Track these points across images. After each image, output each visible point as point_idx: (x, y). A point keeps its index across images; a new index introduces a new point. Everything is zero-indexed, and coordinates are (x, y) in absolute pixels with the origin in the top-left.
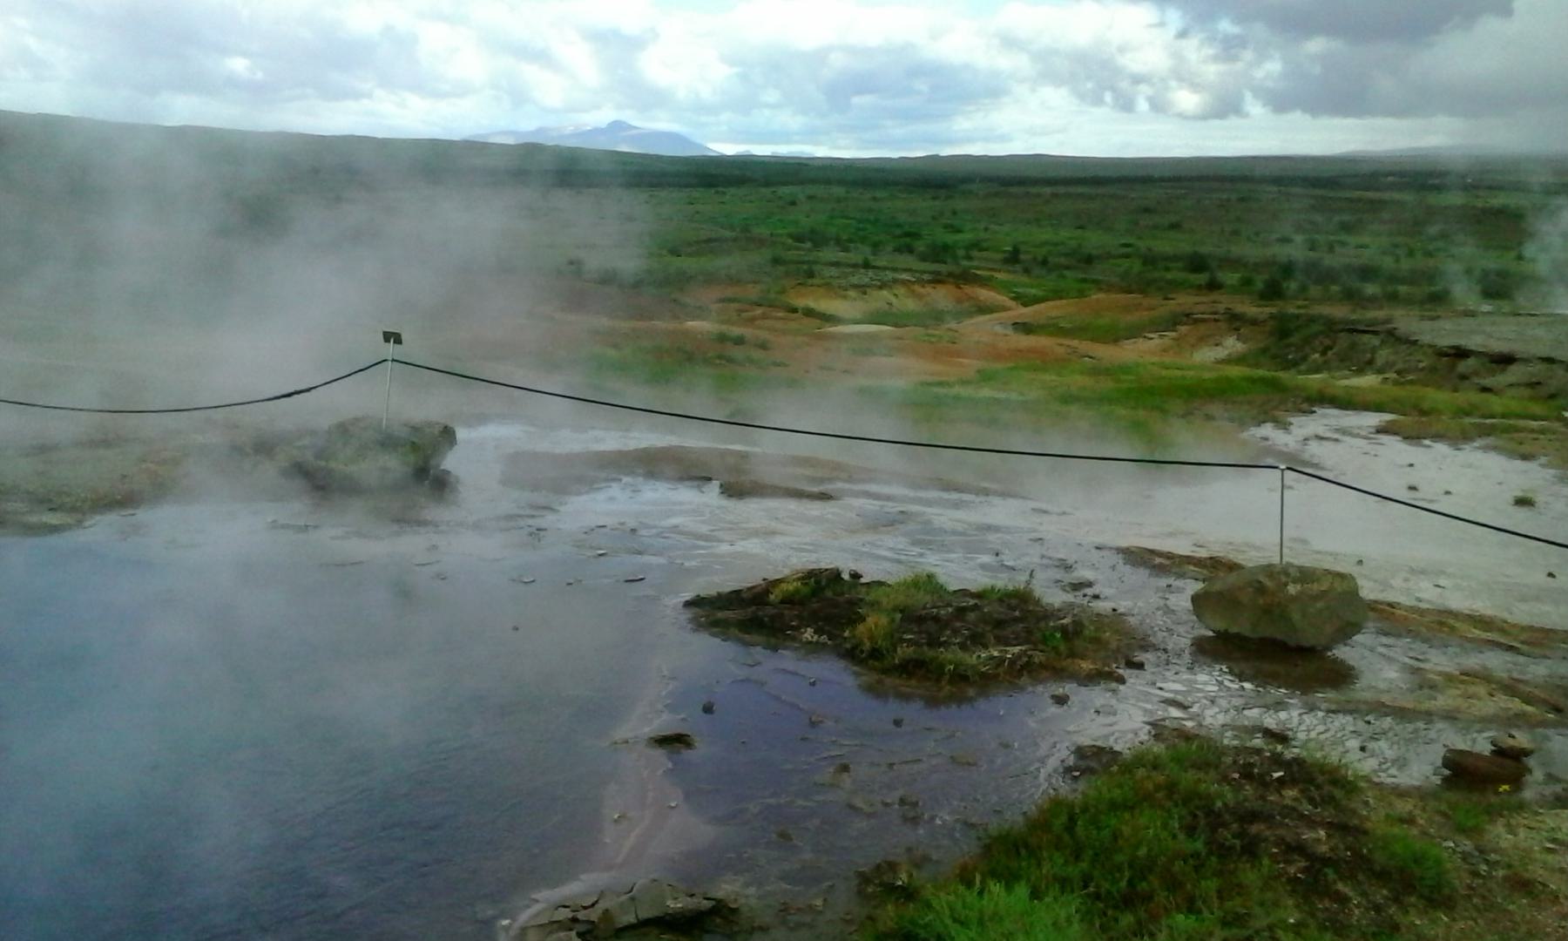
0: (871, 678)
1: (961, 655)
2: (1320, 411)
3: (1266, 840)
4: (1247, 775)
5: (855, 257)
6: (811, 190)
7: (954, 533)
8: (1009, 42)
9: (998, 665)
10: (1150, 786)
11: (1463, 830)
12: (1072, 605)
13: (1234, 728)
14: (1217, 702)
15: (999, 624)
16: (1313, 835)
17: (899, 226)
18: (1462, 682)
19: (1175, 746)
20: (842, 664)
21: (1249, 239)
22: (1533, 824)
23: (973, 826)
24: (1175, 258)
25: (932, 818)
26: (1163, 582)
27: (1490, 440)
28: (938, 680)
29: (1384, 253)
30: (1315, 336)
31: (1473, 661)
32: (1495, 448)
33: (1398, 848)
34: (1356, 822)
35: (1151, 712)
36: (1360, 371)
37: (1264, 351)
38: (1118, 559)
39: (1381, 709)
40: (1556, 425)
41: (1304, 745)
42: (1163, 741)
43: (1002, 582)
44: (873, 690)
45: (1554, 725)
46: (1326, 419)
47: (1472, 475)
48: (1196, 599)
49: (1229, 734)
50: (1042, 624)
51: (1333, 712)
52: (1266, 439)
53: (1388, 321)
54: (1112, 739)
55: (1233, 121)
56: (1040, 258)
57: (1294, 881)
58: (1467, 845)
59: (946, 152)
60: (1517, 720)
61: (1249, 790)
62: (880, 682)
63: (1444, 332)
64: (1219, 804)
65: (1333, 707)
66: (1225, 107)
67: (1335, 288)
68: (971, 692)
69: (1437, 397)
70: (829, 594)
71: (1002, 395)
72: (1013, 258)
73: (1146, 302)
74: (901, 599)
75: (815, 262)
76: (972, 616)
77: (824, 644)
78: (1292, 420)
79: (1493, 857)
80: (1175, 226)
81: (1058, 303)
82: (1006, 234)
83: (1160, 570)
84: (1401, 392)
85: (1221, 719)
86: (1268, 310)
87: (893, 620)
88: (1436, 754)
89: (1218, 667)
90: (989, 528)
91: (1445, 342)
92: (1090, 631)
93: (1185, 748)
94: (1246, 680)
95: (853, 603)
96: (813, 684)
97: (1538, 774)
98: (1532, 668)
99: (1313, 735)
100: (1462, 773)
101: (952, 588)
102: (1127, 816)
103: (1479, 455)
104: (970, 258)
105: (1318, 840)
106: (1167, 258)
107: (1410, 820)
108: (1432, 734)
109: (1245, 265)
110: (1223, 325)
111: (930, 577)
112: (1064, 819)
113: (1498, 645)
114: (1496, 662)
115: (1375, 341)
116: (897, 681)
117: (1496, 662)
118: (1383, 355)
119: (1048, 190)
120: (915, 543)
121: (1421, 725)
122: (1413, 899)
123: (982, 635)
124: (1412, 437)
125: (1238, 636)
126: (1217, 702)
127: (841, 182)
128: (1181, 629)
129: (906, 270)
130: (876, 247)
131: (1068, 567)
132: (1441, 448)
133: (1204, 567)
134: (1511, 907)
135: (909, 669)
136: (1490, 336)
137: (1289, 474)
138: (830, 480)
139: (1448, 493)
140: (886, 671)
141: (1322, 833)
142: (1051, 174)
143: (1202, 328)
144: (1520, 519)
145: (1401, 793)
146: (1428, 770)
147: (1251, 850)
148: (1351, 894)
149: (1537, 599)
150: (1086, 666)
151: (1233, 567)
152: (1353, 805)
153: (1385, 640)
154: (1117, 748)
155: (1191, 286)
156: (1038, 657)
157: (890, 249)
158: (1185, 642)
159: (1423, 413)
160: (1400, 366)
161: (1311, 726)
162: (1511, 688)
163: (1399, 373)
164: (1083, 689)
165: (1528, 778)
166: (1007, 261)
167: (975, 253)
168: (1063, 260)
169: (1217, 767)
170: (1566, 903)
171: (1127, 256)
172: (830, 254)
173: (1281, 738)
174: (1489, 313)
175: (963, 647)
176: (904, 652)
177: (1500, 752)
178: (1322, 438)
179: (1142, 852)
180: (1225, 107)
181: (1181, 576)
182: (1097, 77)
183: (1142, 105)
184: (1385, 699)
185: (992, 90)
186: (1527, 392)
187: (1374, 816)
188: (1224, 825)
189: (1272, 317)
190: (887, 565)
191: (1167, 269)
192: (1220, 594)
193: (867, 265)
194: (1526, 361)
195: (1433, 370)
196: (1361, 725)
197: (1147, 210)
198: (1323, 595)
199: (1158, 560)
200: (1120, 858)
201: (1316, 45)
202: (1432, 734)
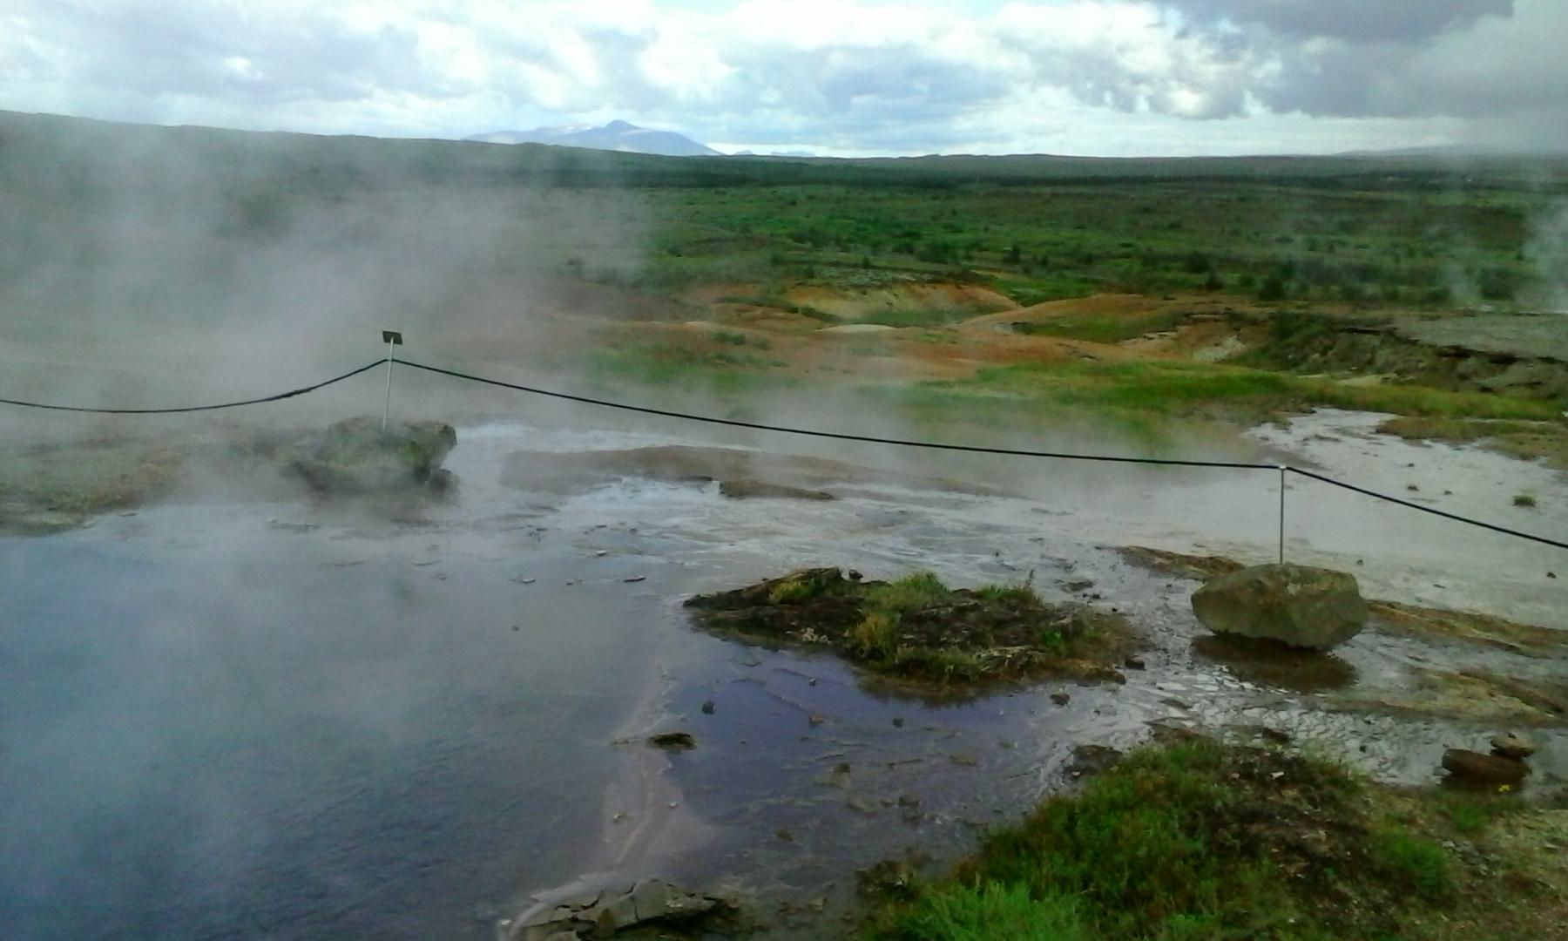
0: (871, 678)
1: (961, 655)
2: (1320, 411)
3: (1266, 840)
4: (1247, 775)
5: (855, 257)
6: (811, 190)
7: (954, 533)
8: (1009, 42)
9: (998, 665)
10: (1150, 786)
11: (1463, 830)
12: (1072, 605)
13: (1234, 728)
14: (1217, 702)
15: (999, 624)
16: (1313, 835)
17: (899, 226)
18: (1462, 682)
19: (1175, 746)
20: (842, 664)
21: (1249, 239)
22: (1533, 824)
23: (973, 826)
24: (1175, 258)
25: (932, 818)
26: (1163, 582)
27: (1490, 440)
28: (938, 680)
29: (1384, 253)
31: (1473, 661)
32: (1495, 448)
33: (1398, 848)
34: (1356, 822)
35: (1151, 712)
36: (1360, 371)
37: (1264, 351)
38: (1118, 559)
39: (1381, 709)
40: (1556, 425)
41: (1304, 745)
42: (1163, 741)
43: (1002, 582)
44: (873, 690)
45: (1554, 725)
46: (1326, 419)
47: (1472, 475)
48: (1196, 599)
49: (1229, 734)
50: (1042, 624)
51: (1333, 712)
52: (1266, 439)
53: (1388, 321)
54: (1112, 739)
55: (1233, 121)
56: (1040, 258)
57: (1294, 881)
58: (1467, 845)
59: (946, 152)
60: (1517, 720)
61: (1249, 790)
62: (880, 682)
63: (1444, 332)
64: (1219, 804)
65: (1333, 707)
66: (1225, 107)
67: (1335, 288)
68: (971, 692)
69: (1437, 397)
70: (829, 594)
71: (1002, 395)
72: (1013, 258)
73: (1146, 302)
74: (901, 599)
75: (815, 262)
76: (972, 616)
77: (824, 644)
78: (1292, 420)
79: (1493, 857)
80: (1175, 226)
81: (1058, 303)
82: (1006, 234)
83: (1160, 570)
84: (1401, 392)
85: (1221, 719)
87: (893, 620)
88: (1436, 754)
89: (1218, 667)
90: (989, 528)
91: (1445, 342)
92: (1090, 631)
93: (1185, 748)
94: (1246, 680)
95: (853, 603)
96: (813, 684)
97: (1538, 774)
98: (1532, 668)
99: (1313, 735)
100: (1462, 773)
101: (952, 588)
102: (1127, 816)
103: (1479, 455)
104: (970, 258)
105: (1318, 840)
106: (1167, 258)
107: (1410, 820)
108: (1432, 734)
109: (1245, 265)
110: (1223, 325)
111: (930, 577)
112: (1064, 819)
113: (1498, 645)
114: (1496, 662)
115: (1375, 341)
116: (897, 681)
117: (1496, 662)
118: (1383, 355)
119: (1048, 190)
120: (915, 543)
121: (1421, 725)
122: (1413, 899)
123: (982, 635)
124: (1412, 437)
125: (1238, 636)
126: (1217, 702)
127: (841, 182)
128: (1181, 629)
129: (906, 270)
130: (876, 247)
131: (1068, 567)
132: (1441, 448)
133: (1204, 567)
134: (1511, 907)
135: (909, 669)
136: (1490, 336)
137: (1289, 474)
138: (830, 480)
139: (1448, 493)
140: (886, 671)
141: (1322, 833)
142: (1051, 174)
143: (1202, 328)
144: (1520, 519)
145: (1401, 793)
146: (1428, 770)
147: (1251, 850)
148: (1351, 894)
149: (1537, 599)
150: (1086, 666)
151: (1233, 567)
152: (1353, 805)
153: (1385, 640)
154: (1117, 748)
155: (1191, 286)
156: (1038, 657)
157: (890, 249)
158: (1185, 642)
159: (1423, 413)
160: (1400, 366)
161: (1311, 726)
162: (1511, 688)
163: (1399, 373)
164: (1083, 689)
165: (1528, 778)
166: (1007, 261)
167: (975, 253)
168: (1063, 260)
169: (1217, 767)
171: (1127, 256)
172: (830, 254)
173: (1281, 738)
174: (1489, 313)
175: (963, 647)
176: (904, 652)
177: (1500, 752)
178: (1322, 438)
179: (1142, 852)
180: (1225, 107)
181: (1181, 576)
182: (1097, 77)
183: (1142, 105)
184: (1385, 699)
185: (992, 90)
186: (1527, 392)
187: (1374, 816)
188: (1224, 825)
189: (1272, 317)
190: (887, 565)
191: (1167, 269)
192: (1220, 594)
193: (867, 265)
194: (1526, 361)
195: (1433, 370)
196: (1361, 725)
197: (1147, 210)
198: (1323, 595)
199: (1158, 560)
200: (1120, 858)
201: (1316, 45)
202: (1432, 734)
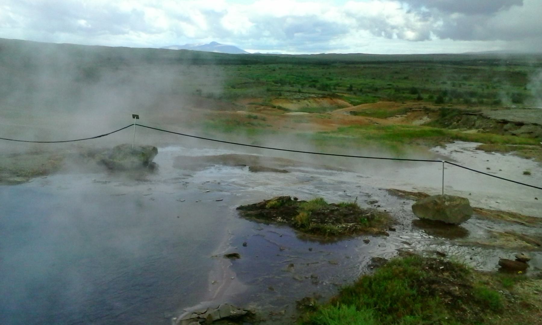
0: (301, 234)
1: (332, 226)
2: (456, 142)
3: (438, 290)
4: (431, 268)
5: (295, 89)
6: (280, 65)
7: (330, 184)
8: (349, 15)
9: (345, 230)
10: (398, 272)
11: (506, 287)
12: (370, 209)
13: (427, 251)
14: (421, 242)
15: (345, 215)
16: (454, 288)
17: (311, 78)
18: (506, 236)
19: (406, 258)
20: (291, 229)
21: (432, 83)
22: (530, 285)
23: (336, 285)
24: (406, 89)
25: (322, 283)
26: (402, 201)
27: (515, 152)
28: (324, 235)
29: (478, 87)
30: (455, 116)
31: (509, 228)
32: (517, 155)
33: (483, 293)
34: (469, 284)
35: (398, 246)
36: (470, 128)
37: (437, 121)
38: (387, 193)
39: (477, 245)
40: (538, 147)
41: (451, 257)
42: (402, 256)
43: (346, 201)
44: (302, 238)
45: (537, 250)
46: (458, 145)
47: (509, 164)
48: (413, 207)
49: (425, 253)
50: (360, 216)
51: (461, 246)
52: (438, 152)
53: (480, 111)
54: (384, 255)
55: (426, 42)
56: (359, 89)
57: (447, 304)
58: (507, 292)
59: (327, 52)
60: (524, 249)
61: (432, 273)
62: (304, 235)
63: (499, 115)
64: (421, 278)
65: (461, 244)
66: (424, 37)
67: (461, 100)
68: (336, 239)
69: (497, 137)
70: (286, 205)
71: (346, 137)
72: (350, 89)
73: (396, 104)
74: (311, 207)
75: (282, 91)
76: (336, 213)
77: (285, 223)
78: (446, 145)
79: (516, 296)
80: (406, 78)
81: (366, 105)
82: (348, 81)
83: (401, 197)
84: (484, 135)
85: (422, 248)
86: (438, 107)
87: (309, 214)
88: (496, 260)
89: (421, 230)
90: (342, 182)
91: (500, 118)
92: (377, 218)
93: (410, 258)
94: (431, 235)
95: (295, 208)
96: (281, 236)
97: (532, 267)
98: (530, 231)
99: (454, 254)
100: (505, 267)
101: (329, 203)
102: (390, 282)
103: (511, 157)
104: (335, 89)
105: (456, 290)
106: (403, 89)
107: (487, 283)
108: (495, 254)
109: (430, 92)
110: (423, 112)
111: (322, 199)
112: (368, 283)
113: (518, 223)
114: (517, 229)
115: (475, 118)
116: (310, 235)
117: (517, 229)
118: (478, 123)
119: (362, 66)
120: (316, 188)
121: (491, 250)
122: (488, 311)
123: (340, 219)
124: (488, 151)
125: (428, 220)
126: (421, 242)
127: (291, 63)
128: (408, 217)
129: (313, 93)
130: (303, 85)
131: (369, 196)
132: (498, 155)
133: (416, 196)
134: (522, 313)
135: (314, 231)
136: (515, 116)
137: (445, 164)
138: (287, 166)
139: (500, 170)
140: (306, 232)
141: (457, 288)
142: (363, 60)
143: (416, 113)
144: (525, 179)
145: (484, 274)
146: (494, 266)
147: (432, 293)
148: (467, 309)
149: (531, 207)
150: (375, 230)
151: (426, 196)
152: (468, 278)
153: (479, 221)
154: (386, 258)
155: (412, 99)
156: (359, 227)
157: (307, 86)
158: (410, 222)
159: (492, 143)
160: (484, 126)
161: (453, 251)
162: (522, 238)
163: (483, 129)
164: (374, 238)
165: (528, 269)
166: (348, 90)
167: (337, 87)
168: (367, 90)
169: (421, 265)
170: (541, 312)
171: (390, 88)
172: (287, 88)
173: (443, 255)
174: (515, 108)
175: (333, 223)
176: (312, 225)
177: (519, 260)
178: (457, 151)
179: (395, 294)
180: (424, 37)
181: (408, 199)
182: (379, 27)
183: (395, 36)
184: (479, 241)
185: (343, 31)
186: (528, 135)
187: (475, 282)
188: (423, 285)
189: (440, 109)
190: (307, 195)
191: (404, 93)
192: (422, 205)
193: (300, 92)
194: (527, 125)
195: (495, 128)
196: (470, 251)
197: (396, 73)
198: (457, 205)
199: (400, 194)
200: (387, 296)
201: (455, 16)
202: (495, 254)
